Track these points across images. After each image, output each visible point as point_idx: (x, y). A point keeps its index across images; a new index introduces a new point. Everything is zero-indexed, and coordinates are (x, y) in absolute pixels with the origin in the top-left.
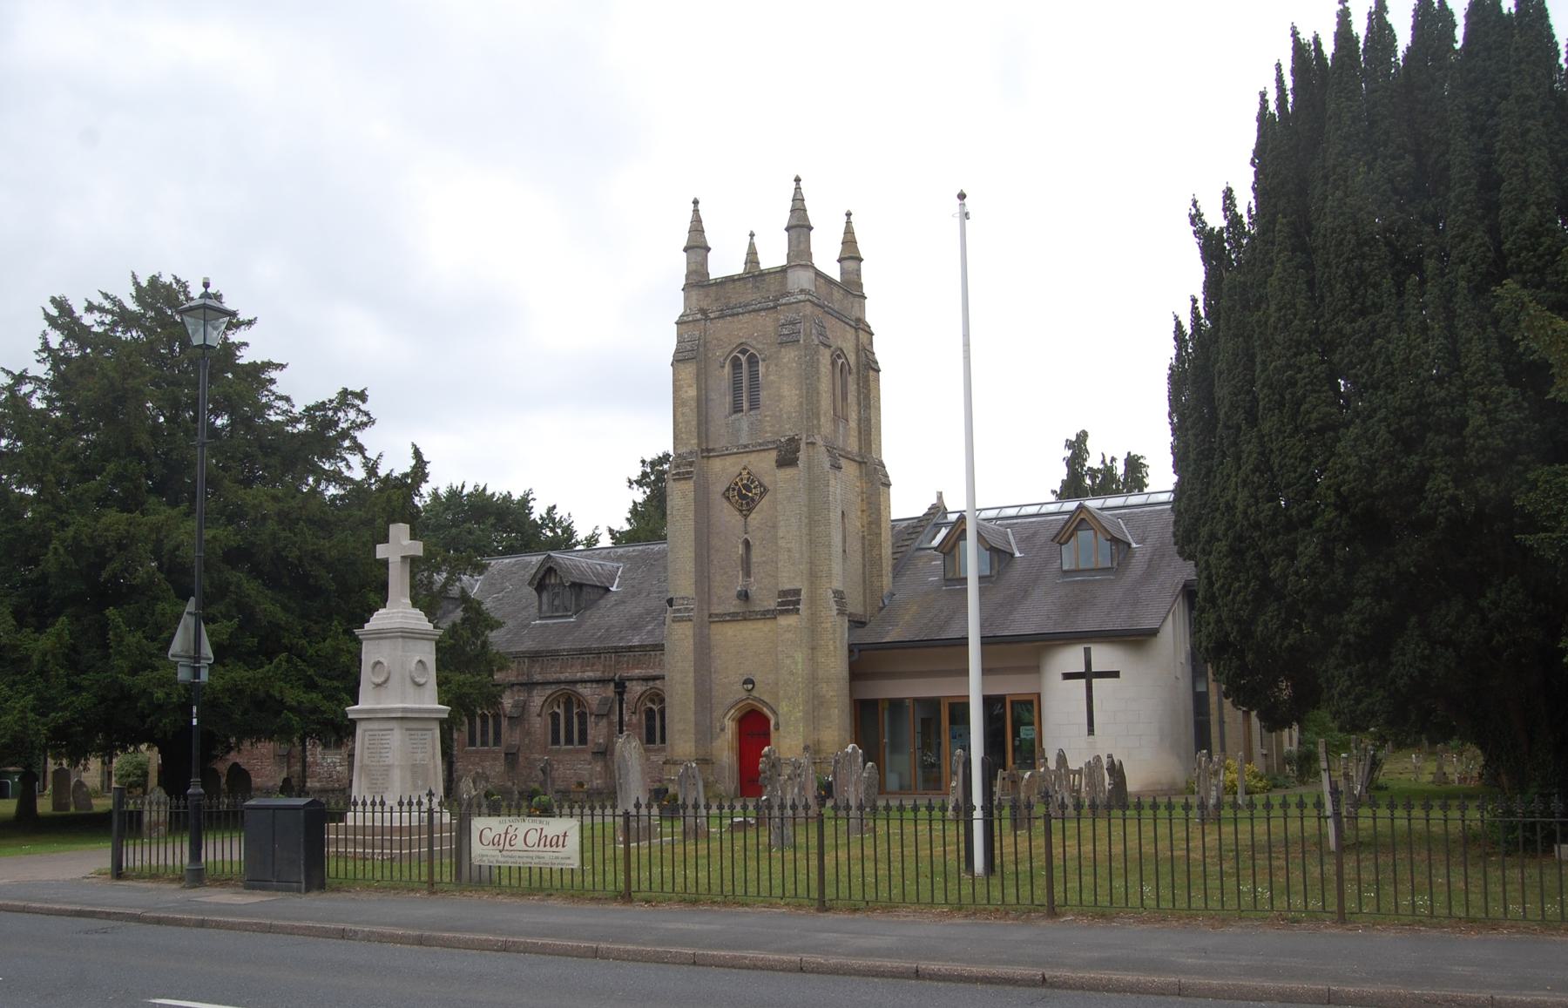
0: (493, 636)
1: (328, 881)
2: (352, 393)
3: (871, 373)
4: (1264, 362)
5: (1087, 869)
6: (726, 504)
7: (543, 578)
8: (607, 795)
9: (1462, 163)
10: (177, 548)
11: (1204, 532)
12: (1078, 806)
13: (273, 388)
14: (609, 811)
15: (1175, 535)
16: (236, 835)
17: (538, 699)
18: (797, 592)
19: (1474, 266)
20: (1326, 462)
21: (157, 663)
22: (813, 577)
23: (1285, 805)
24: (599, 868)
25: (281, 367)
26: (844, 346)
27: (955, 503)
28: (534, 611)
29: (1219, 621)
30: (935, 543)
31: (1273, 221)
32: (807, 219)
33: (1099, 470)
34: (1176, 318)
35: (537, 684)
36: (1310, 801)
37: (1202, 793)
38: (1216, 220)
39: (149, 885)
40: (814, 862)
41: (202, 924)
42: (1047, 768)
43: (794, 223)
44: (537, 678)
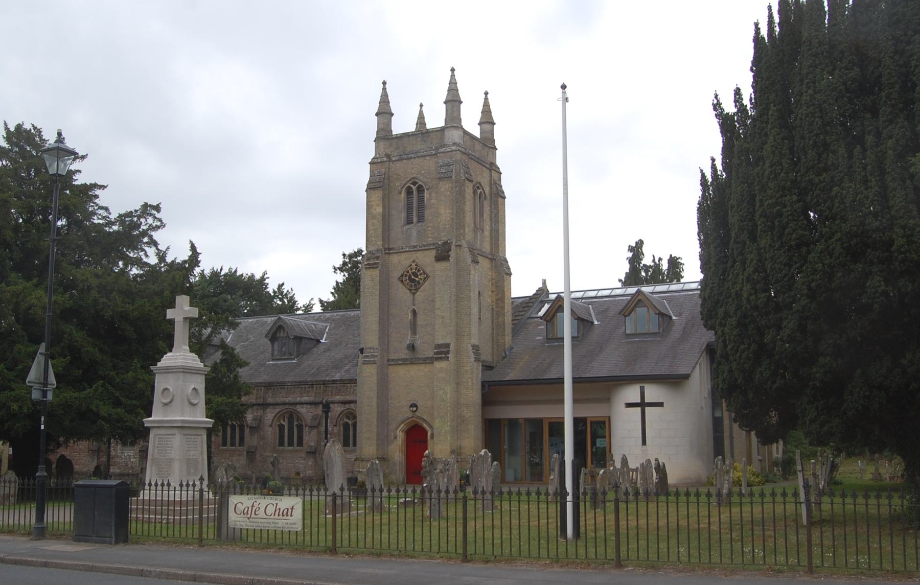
0: (242, 372)
1: (130, 537)
2: (151, 206)
3: (500, 199)
4: (761, 201)
5: (643, 536)
6: (401, 285)
7: (275, 333)
8: (321, 481)
9: (889, 73)
10: (30, 308)
11: (721, 311)
12: (637, 493)
13: (97, 201)
14: (322, 492)
15: (702, 313)
16: (68, 504)
17: (270, 415)
18: (448, 345)
19: (897, 141)
20: (801, 266)
21: (13, 385)
22: (459, 335)
23: (773, 494)
24: (315, 530)
25: (103, 187)
26: (482, 181)
27: (555, 287)
28: (268, 355)
29: (730, 371)
30: (541, 313)
31: (768, 109)
32: (458, 95)
33: (650, 267)
34: (702, 171)
35: (270, 404)
36: (790, 492)
37: (718, 486)
38: (730, 108)
39: (8, 538)
40: (460, 529)
41: (45, 565)
42: (615, 467)
43: (450, 98)
44: (270, 400)
